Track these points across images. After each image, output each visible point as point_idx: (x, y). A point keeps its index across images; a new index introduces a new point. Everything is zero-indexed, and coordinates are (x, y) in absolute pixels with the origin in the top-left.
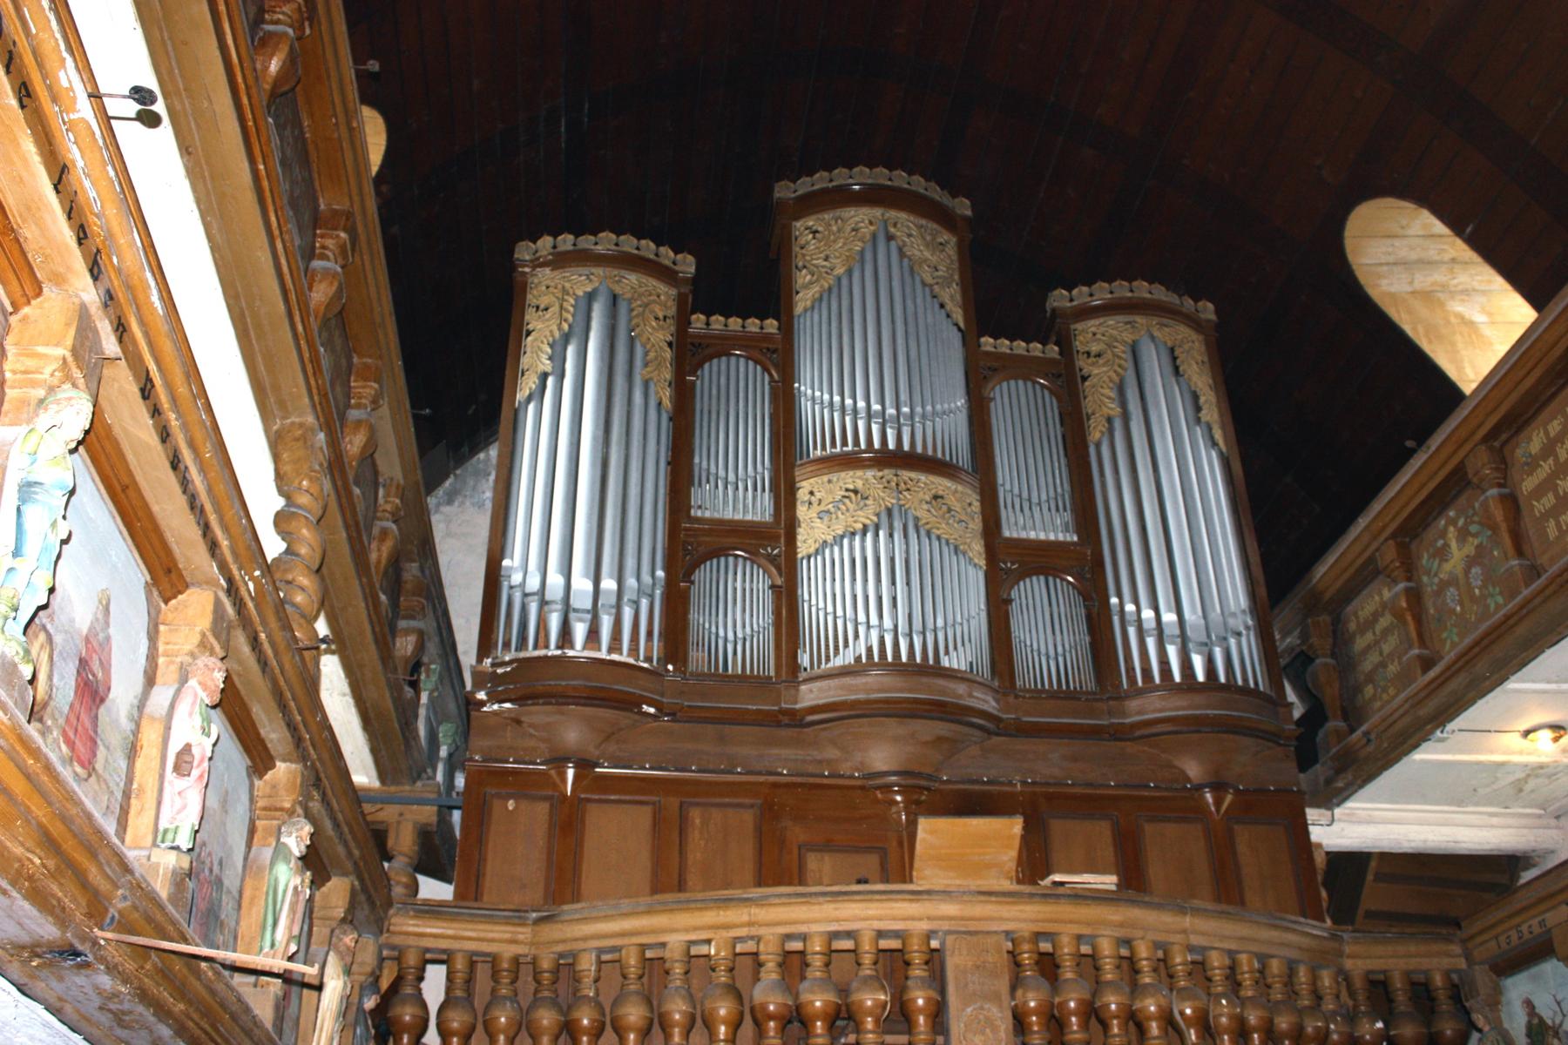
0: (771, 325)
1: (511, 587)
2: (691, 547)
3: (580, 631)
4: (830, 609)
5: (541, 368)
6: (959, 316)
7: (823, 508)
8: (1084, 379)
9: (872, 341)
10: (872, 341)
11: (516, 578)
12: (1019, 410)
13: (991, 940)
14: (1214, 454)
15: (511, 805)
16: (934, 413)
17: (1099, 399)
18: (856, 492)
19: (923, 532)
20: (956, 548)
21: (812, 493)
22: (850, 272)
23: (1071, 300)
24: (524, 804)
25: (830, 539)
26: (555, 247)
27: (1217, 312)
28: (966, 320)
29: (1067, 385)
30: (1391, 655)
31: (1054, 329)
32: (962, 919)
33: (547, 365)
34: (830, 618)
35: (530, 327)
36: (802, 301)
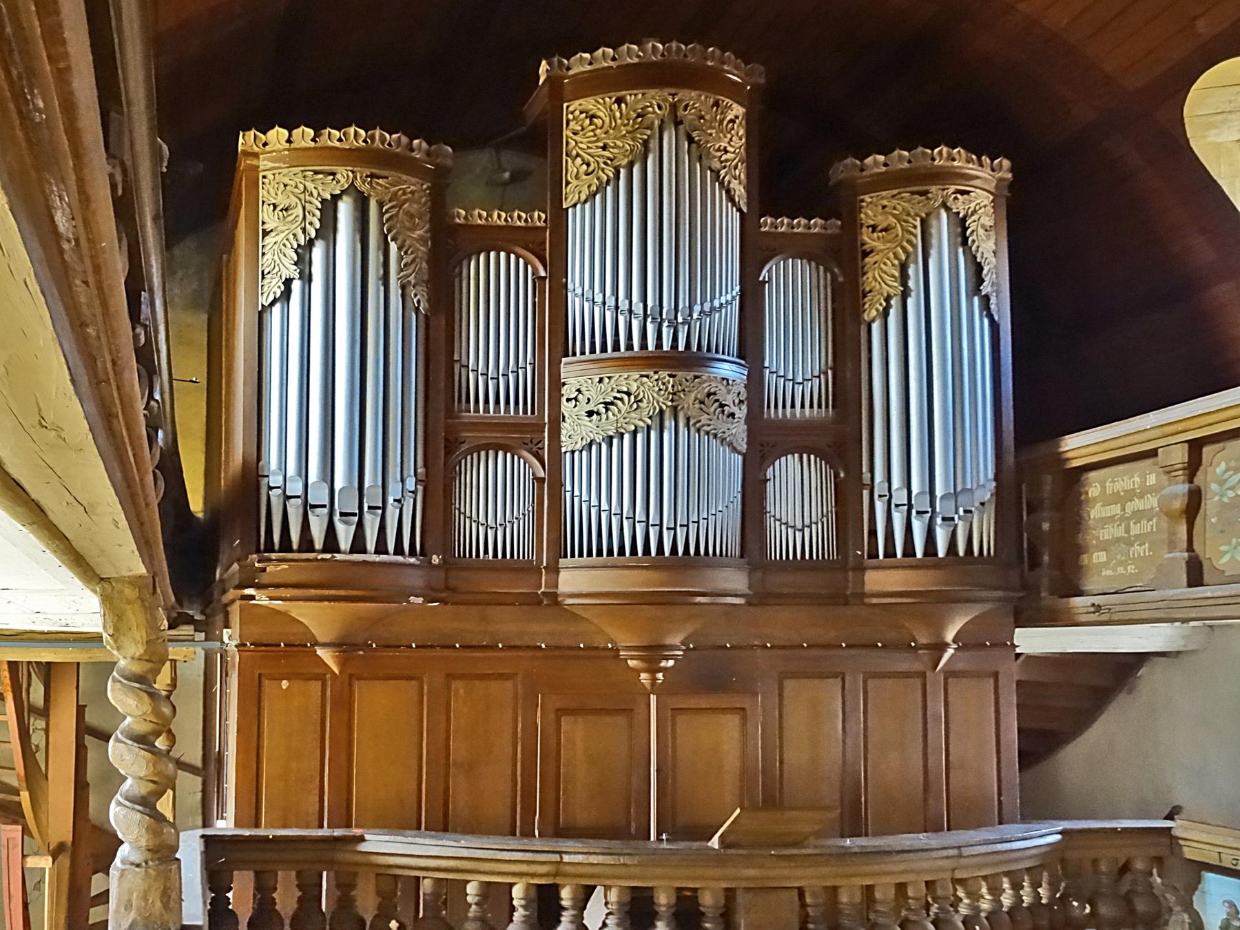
0: (538, 218)
1: (271, 488)
2: (447, 433)
3: (345, 535)
4: (594, 502)
5: (285, 274)
6: (739, 190)
7: (591, 407)
8: (866, 254)
9: (640, 204)
10: (640, 204)
11: (276, 480)
12: (793, 287)
13: (784, 895)
14: (986, 321)
15: (285, 684)
16: (713, 309)
17: (879, 277)
18: (628, 394)
19: (692, 430)
20: (723, 440)
21: (579, 391)
22: (630, 166)
23: (862, 170)
24: (298, 684)
25: (599, 439)
26: (289, 141)
27: (1012, 170)
28: (748, 204)
29: (842, 262)
30: (1137, 536)
31: (840, 205)
32: (761, 879)
33: (293, 272)
34: (594, 511)
35: (268, 227)
36: (571, 194)
